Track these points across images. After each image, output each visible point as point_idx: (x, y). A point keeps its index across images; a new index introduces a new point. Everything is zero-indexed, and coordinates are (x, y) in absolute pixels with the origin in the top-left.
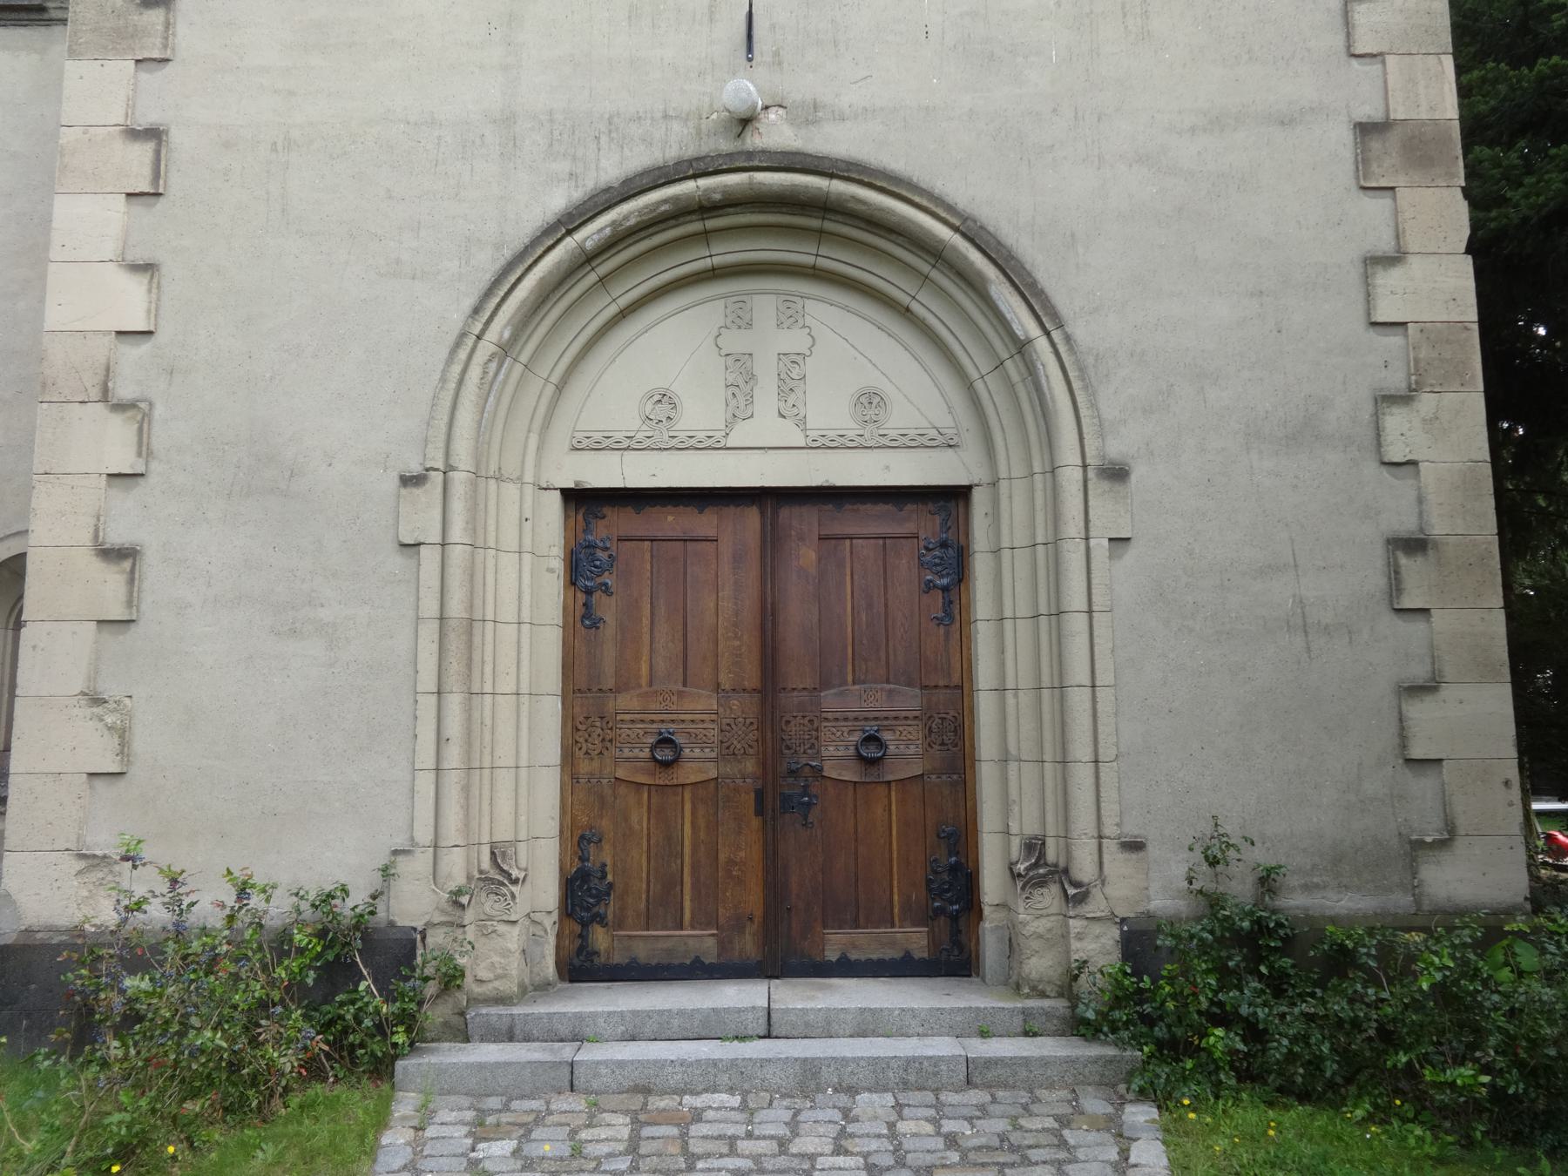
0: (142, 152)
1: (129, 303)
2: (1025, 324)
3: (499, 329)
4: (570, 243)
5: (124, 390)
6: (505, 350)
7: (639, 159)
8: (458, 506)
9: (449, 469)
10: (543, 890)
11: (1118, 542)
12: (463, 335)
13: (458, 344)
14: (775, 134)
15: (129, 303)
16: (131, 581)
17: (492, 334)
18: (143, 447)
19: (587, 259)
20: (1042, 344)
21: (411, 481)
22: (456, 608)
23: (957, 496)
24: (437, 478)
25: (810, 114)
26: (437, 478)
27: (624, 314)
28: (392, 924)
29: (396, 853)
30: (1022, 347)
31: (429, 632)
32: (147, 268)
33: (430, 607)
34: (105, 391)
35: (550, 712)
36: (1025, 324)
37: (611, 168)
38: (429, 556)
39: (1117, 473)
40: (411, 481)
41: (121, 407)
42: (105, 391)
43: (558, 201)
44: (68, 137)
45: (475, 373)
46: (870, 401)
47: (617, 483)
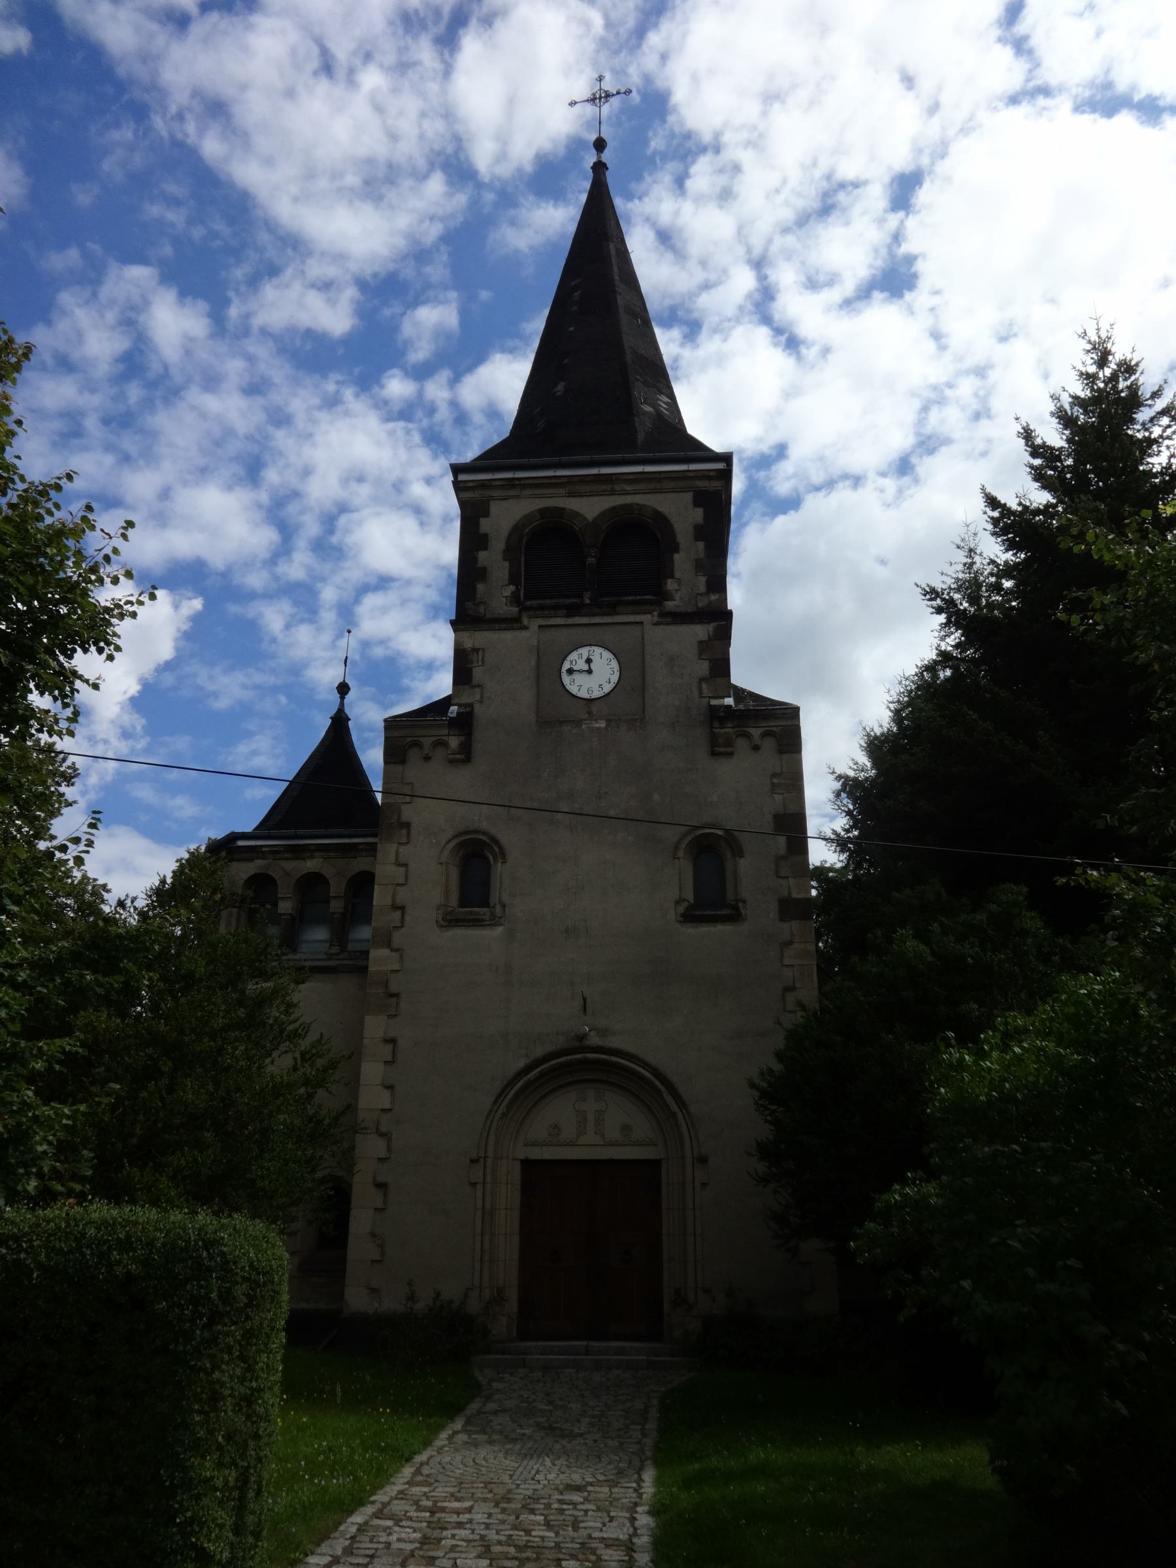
0: (389, 1047)
1: (384, 1100)
2: (674, 1107)
3: (502, 1109)
4: (525, 1079)
5: (383, 1129)
6: (504, 1115)
7: (549, 1048)
8: (489, 1170)
9: (486, 1157)
10: (512, 1305)
11: (704, 1185)
12: (491, 1111)
13: (488, 1115)
14: (594, 1040)
15: (384, 1100)
16: (385, 1195)
17: (500, 1111)
18: (389, 1149)
19: (529, 1084)
20: (680, 1115)
21: (474, 1161)
22: (488, 1206)
23: (655, 1164)
24: (482, 1160)
25: (603, 1033)
26: (482, 1160)
27: (543, 1097)
28: (771, 488)
29: (1038, 65)
30: (674, 1114)
31: (479, 1213)
32: (390, 1087)
33: (480, 1205)
34: (377, 1129)
35: (516, 1239)
36: (674, 1107)
37: (539, 1052)
38: (480, 1187)
39: (703, 1160)
40: (474, 1161)
41: (382, 1135)
42: (377, 1129)
43: (522, 1063)
44: (366, 1041)
45: (495, 1124)
46: (626, 1128)
47: (539, 1157)
